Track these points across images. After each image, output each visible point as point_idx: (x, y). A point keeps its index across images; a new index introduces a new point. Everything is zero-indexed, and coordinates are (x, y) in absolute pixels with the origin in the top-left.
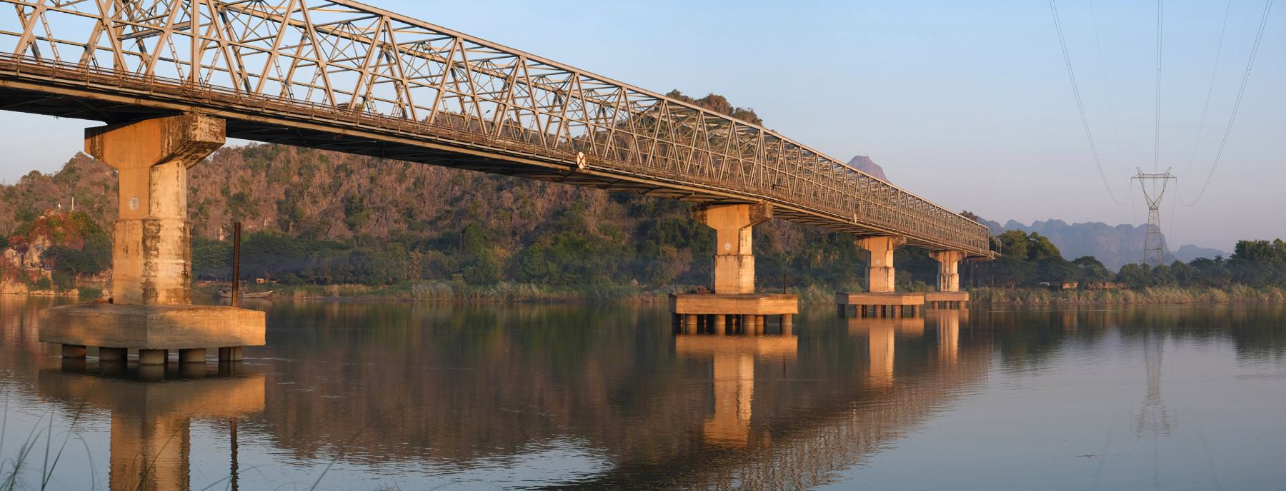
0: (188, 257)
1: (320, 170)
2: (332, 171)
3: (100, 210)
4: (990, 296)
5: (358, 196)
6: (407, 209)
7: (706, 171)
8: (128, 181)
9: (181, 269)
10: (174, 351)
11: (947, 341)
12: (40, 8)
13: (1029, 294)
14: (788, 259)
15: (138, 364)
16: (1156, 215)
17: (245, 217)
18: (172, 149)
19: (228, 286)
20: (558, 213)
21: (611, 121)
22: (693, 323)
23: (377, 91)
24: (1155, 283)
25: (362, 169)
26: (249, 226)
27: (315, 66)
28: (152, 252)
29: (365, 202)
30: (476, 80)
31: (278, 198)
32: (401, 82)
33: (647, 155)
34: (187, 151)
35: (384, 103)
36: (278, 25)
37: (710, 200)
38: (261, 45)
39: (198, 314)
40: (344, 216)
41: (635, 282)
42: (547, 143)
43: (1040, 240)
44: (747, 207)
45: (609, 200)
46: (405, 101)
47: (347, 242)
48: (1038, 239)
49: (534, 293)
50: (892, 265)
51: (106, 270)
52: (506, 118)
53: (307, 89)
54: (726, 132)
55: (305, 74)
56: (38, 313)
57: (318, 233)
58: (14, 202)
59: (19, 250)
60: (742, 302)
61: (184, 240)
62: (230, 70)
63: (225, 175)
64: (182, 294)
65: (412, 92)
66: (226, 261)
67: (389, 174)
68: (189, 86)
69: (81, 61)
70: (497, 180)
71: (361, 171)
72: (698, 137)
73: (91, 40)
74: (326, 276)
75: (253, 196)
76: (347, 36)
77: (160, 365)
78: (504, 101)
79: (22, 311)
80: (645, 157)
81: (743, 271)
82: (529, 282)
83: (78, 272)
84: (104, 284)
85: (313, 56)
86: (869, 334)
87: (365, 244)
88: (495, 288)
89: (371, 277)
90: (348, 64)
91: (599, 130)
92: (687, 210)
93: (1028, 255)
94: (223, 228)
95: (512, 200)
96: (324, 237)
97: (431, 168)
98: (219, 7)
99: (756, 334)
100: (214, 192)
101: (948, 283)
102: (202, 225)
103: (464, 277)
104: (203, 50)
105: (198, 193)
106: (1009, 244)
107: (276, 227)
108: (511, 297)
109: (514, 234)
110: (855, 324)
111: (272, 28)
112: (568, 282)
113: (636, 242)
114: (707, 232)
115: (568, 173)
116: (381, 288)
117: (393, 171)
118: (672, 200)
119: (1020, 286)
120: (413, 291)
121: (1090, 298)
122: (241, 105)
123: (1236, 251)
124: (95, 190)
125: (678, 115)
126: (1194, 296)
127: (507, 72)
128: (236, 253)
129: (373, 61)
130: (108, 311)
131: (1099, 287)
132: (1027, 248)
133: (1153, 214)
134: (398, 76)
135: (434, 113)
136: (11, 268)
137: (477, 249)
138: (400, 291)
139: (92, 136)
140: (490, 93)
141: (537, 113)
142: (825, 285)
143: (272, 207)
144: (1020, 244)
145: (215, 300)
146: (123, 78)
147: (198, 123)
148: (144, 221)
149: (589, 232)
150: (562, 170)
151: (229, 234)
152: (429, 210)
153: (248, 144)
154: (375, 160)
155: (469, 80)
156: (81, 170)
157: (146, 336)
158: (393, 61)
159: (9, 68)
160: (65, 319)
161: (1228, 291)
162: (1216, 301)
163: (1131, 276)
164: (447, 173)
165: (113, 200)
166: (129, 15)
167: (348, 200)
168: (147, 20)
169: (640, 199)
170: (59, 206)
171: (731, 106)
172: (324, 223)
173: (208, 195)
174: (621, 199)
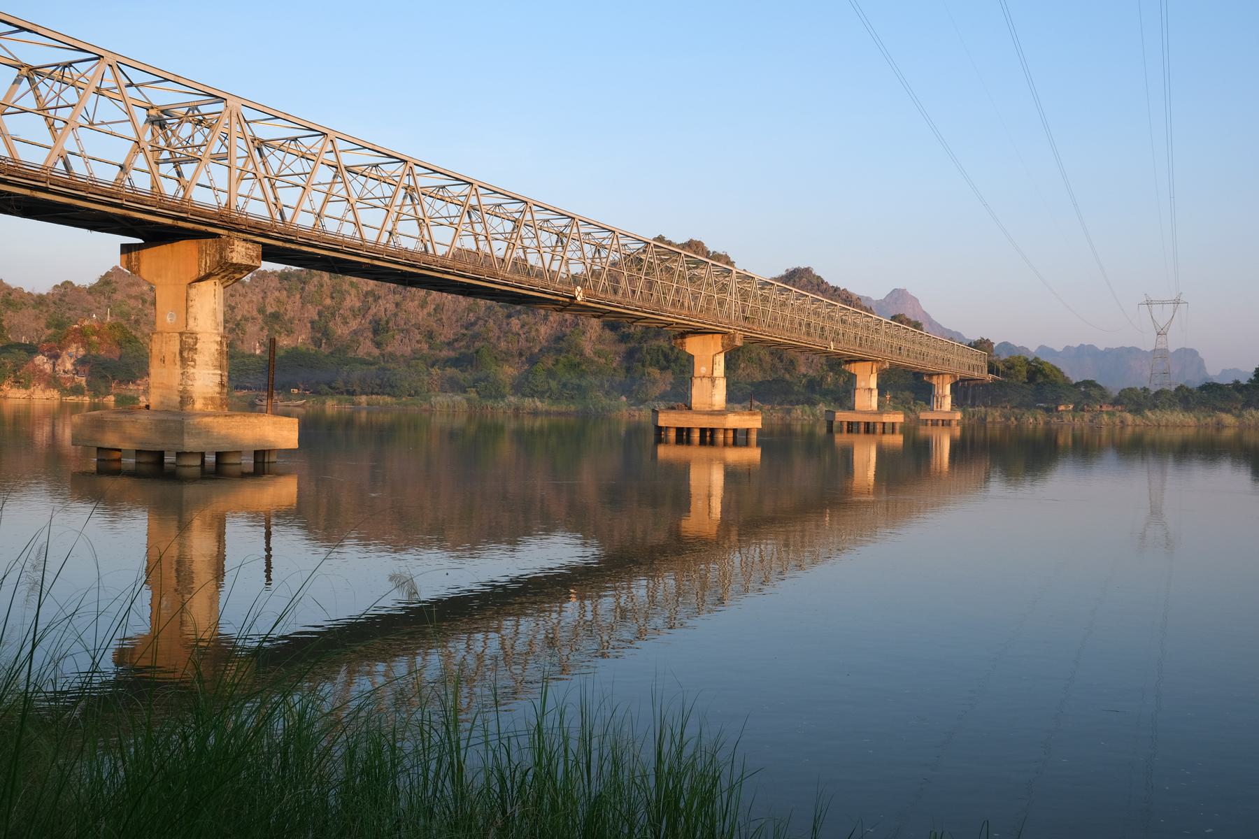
0: (225, 367)
1: (350, 295)
2: (361, 296)
3: (137, 322)
5: (385, 319)
6: (428, 331)
7: (686, 305)
8: (166, 296)
9: (218, 379)
10: (210, 453)
11: (938, 455)
12: (71, 124)
13: (1024, 414)
14: (804, 380)
15: (175, 466)
16: (1164, 339)
17: (280, 333)
18: (209, 269)
19: (263, 395)
20: (559, 338)
21: (605, 260)
22: (672, 435)
23: (402, 227)
24: (1156, 406)
25: (388, 295)
26: (284, 342)
27: (346, 202)
28: (189, 363)
29: (391, 324)
30: (489, 222)
31: (311, 318)
32: (424, 220)
33: (635, 291)
34: (223, 271)
35: (408, 239)
36: (312, 163)
37: (688, 330)
38: (296, 180)
39: (233, 420)
40: (371, 336)
41: (624, 398)
42: (550, 278)
43: (1041, 364)
44: (720, 336)
45: (603, 328)
46: (427, 237)
47: (374, 358)
48: (1039, 364)
50: (875, 387)
51: (143, 378)
52: (514, 255)
53: (339, 222)
54: (704, 271)
55: (337, 208)
56: (71, 418)
57: (348, 350)
58: (44, 310)
59: (50, 357)
60: (713, 417)
61: (221, 353)
62: (266, 200)
63: (261, 295)
64: (218, 402)
65: (433, 229)
66: (262, 372)
67: (412, 300)
68: (226, 212)
69: (116, 180)
70: (507, 308)
71: (387, 297)
72: (679, 275)
73: (127, 160)
74: (354, 388)
75: (288, 316)
76: (375, 177)
77: (196, 466)
78: (513, 241)
79: (55, 416)
80: (634, 292)
81: (715, 391)
82: (533, 396)
83: (114, 379)
84: (140, 392)
85: (343, 193)
87: (390, 360)
88: (503, 401)
89: (396, 390)
90: (376, 202)
91: (595, 268)
92: (669, 338)
93: (1028, 378)
94: (259, 343)
95: (519, 326)
96: (353, 354)
97: (450, 297)
98: (256, 142)
99: (725, 444)
100: (250, 310)
101: (941, 403)
102: (239, 339)
103: (476, 391)
104: (240, 180)
105: (236, 310)
106: (1010, 368)
107: (309, 343)
108: (517, 409)
109: (521, 355)
110: (841, 439)
111: (306, 166)
112: (566, 398)
113: (625, 364)
114: (686, 357)
115: (568, 304)
116: (404, 399)
117: (416, 298)
118: (657, 329)
119: (1016, 407)
120: (433, 403)
121: (1085, 419)
122: (276, 233)
123: (1255, 375)
124: (132, 302)
125: (662, 257)
126: (1198, 420)
127: (517, 215)
128: (271, 366)
129: (399, 201)
130: (143, 417)
131: (1095, 409)
132: (1028, 372)
133: (1162, 339)
134: (421, 215)
135: (452, 249)
136: (42, 374)
137: (489, 367)
138: (422, 402)
139: (128, 252)
140: (501, 234)
141: (541, 252)
142: (832, 404)
143: (306, 326)
144: (1019, 368)
145: (252, 408)
146: (160, 200)
147: (235, 247)
148: (181, 334)
149: (585, 355)
150: (563, 301)
151: (265, 348)
152: (447, 333)
153: (284, 268)
154: (400, 288)
155: (483, 221)
156: (117, 283)
157: (183, 440)
158: (416, 202)
159: (38, 179)
160: (99, 425)
161: (1239, 416)
162: (1223, 425)
163: (1129, 399)
164: (464, 302)
165: (151, 313)
166: (166, 141)
167: (375, 322)
168: (185, 148)
169: (629, 327)
170: (94, 316)
171: (708, 250)
172: (354, 341)
173: (245, 313)
174: (613, 327)
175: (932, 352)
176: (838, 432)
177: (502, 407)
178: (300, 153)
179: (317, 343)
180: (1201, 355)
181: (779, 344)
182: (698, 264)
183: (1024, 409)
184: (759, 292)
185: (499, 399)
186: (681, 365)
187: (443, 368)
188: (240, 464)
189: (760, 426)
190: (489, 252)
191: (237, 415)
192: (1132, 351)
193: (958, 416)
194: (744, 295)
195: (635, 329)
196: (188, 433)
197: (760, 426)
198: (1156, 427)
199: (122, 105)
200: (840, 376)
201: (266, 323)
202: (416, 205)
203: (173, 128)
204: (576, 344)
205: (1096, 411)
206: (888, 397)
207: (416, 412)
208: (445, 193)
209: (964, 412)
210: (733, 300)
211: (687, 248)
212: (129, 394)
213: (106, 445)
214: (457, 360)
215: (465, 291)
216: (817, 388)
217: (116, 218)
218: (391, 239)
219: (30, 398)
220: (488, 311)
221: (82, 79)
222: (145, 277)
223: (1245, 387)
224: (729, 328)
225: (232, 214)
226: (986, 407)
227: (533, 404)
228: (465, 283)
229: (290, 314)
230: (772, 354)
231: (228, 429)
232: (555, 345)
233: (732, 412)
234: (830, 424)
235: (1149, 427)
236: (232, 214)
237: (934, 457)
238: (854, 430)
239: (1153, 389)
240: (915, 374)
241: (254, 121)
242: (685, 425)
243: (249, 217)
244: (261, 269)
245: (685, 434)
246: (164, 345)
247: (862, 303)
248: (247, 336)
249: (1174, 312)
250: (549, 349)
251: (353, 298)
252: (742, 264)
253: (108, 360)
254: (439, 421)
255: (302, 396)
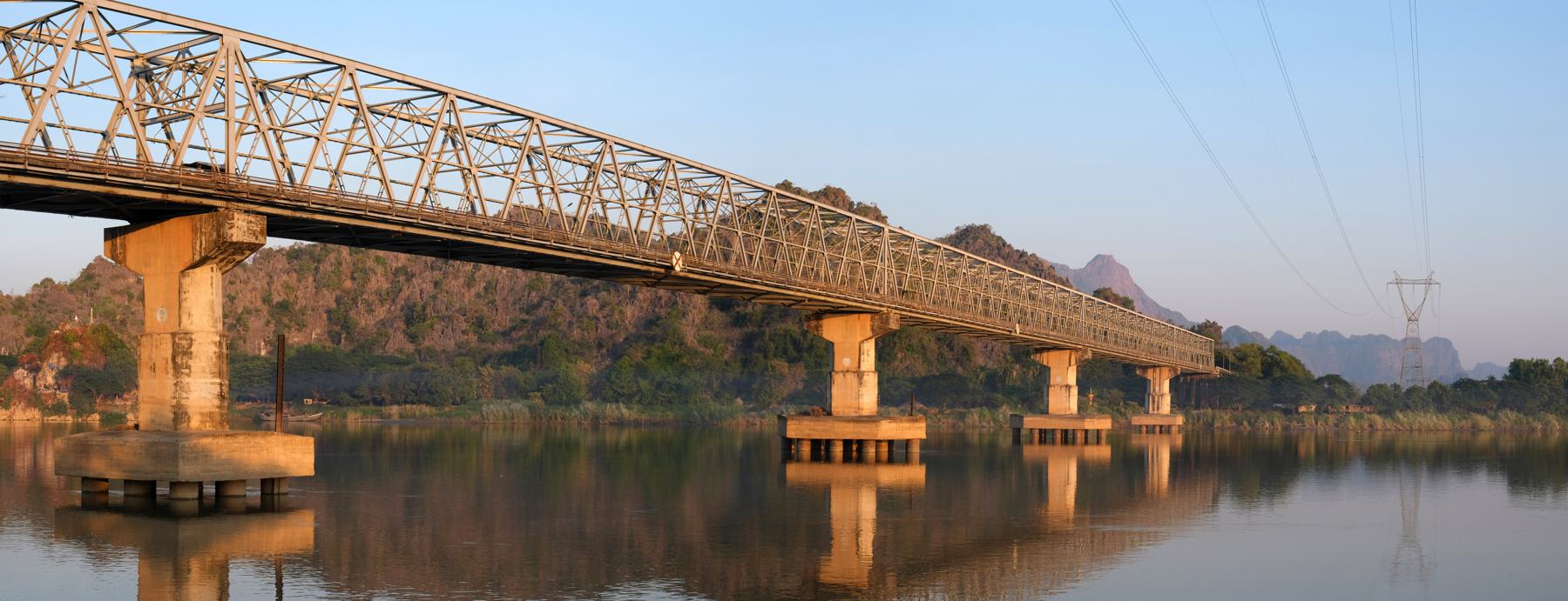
1: (376, 274)
2: (390, 274)
3: (123, 322)
4: (1213, 419)
5: (420, 303)
6: (477, 318)
7: (822, 274)
8: (155, 290)
9: (217, 389)
10: (209, 483)
11: (1156, 473)
12: (50, 90)
13: (1258, 417)
16: (1415, 327)
17: (290, 328)
19: (271, 408)
20: (651, 323)
22: (806, 449)
23: (441, 181)
24: (1408, 407)
26: (295, 339)
28: (183, 371)
29: (428, 311)
30: (556, 168)
32: (470, 170)
34: (222, 253)
35: (450, 196)
36: (326, 106)
38: (307, 129)
39: (236, 440)
40: (403, 326)
41: (739, 401)
43: (1278, 355)
44: (868, 316)
45: (710, 307)
46: (474, 193)
47: (408, 356)
49: (623, 415)
51: (130, 391)
52: (590, 212)
53: (361, 179)
56: (53, 442)
58: (23, 316)
61: (220, 356)
62: (271, 159)
63: (267, 279)
64: (218, 418)
65: (481, 182)
66: (268, 379)
67: (456, 277)
69: (98, 151)
70: (581, 284)
71: (423, 274)
72: (812, 234)
76: (407, 117)
77: (193, 499)
78: (588, 193)
79: (35, 441)
80: (751, 257)
81: (863, 390)
83: (99, 394)
84: (128, 408)
85: (366, 142)
86: (1047, 463)
87: (428, 359)
88: (578, 408)
89: (436, 396)
90: (408, 150)
92: (800, 320)
93: (1263, 372)
95: (597, 307)
96: (381, 351)
97: (504, 271)
98: (258, 85)
99: (878, 461)
100: (254, 300)
103: (542, 395)
105: (236, 301)
106: (1242, 360)
107: (325, 339)
108: (596, 418)
110: (1031, 452)
111: (319, 110)
113: (740, 356)
114: (824, 345)
116: (447, 409)
117: (461, 274)
118: (783, 307)
120: (484, 413)
121: (1330, 423)
122: (284, 199)
124: (117, 299)
125: (789, 210)
126: (1453, 422)
127: (592, 158)
129: (437, 146)
130: (133, 439)
132: (1262, 365)
133: (1413, 326)
141: (626, 206)
142: (1019, 406)
143: (321, 317)
145: (257, 424)
146: (147, 170)
148: (173, 335)
150: (655, 272)
151: (272, 348)
153: (293, 244)
154: (440, 262)
155: (548, 168)
156: (100, 276)
157: (177, 466)
158: (459, 146)
159: (15, 160)
160: (84, 449)
161: (1494, 418)
164: (523, 277)
166: (153, 96)
167: (409, 308)
168: (174, 102)
169: (745, 306)
170: (76, 318)
171: (852, 200)
173: (248, 304)
174: (723, 305)
175: (1146, 338)
176: (1026, 443)
177: (576, 416)
178: (312, 94)
179: (336, 338)
180: (1455, 346)
181: (948, 327)
182: (838, 219)
183: (1258, 411)
184: (920, 258)
185: (572, 406)
186: (817, 356)
187: (497, 366)
188: (245, 496)
189: (924, 437)
190: (556, 209)
191: (240, 434)
192: (1382, 340)
193: (1180, 420)
194: (901, 261)
195: (753, 308)
196: (183, 458)
197: (924, 437)
198: (1409, 432)
199: (103, 58)
200: (1028, 368)
201: (272, 315)
202: (459, 150)
203: (161, 79)
204: (674, 330)
205: (1342, 413)
206: (1091, 396)
207: (463, 425)
208: (497, 133)
209: (1186, 415)
210: (885, 268)
211: (823, 198)
212: (116, 411)
213: (92, 475)
214: (516, 355)
215: (526, 263)
216: (999, 385)
217: (98, 198)
218: (428, 198)
219: (10, 420)
220: (556, 288)
221: (61, 35)
222: (132, 267)
223: (1501, 384)
224: (881, 306)
225: (231, 179)
226: (1213, 409)
227: (617, 412)
228: (526, 251)
229: (302, 303)
230: (939, 339)
231: (230, 452)
232: (646, 332)
233: (886, 418)
234: (1017, 432)
235: (1400, 432)
236: (231, 179)
237: (1150, 470)
238: (1047, 441)
239: (1405, 387)
240: (1125, 366)
241: (255, 59)
242: (824, 437)
243: (252, 182)
244: (266, 247)
245: (823, 448)
246: (154, 349)
247: (1056, 273)
248: (250, 333)
249: (1426, 294)
250: (638, 338)
251: (380, 278)
252: (896, 219)
253: (92, 371)
254: (492, 436)
255: (318, 408)
